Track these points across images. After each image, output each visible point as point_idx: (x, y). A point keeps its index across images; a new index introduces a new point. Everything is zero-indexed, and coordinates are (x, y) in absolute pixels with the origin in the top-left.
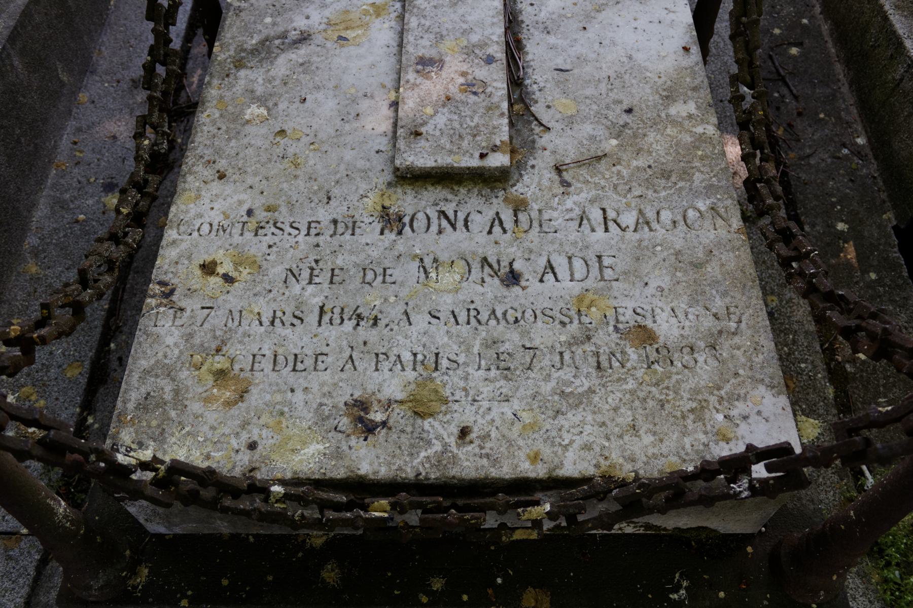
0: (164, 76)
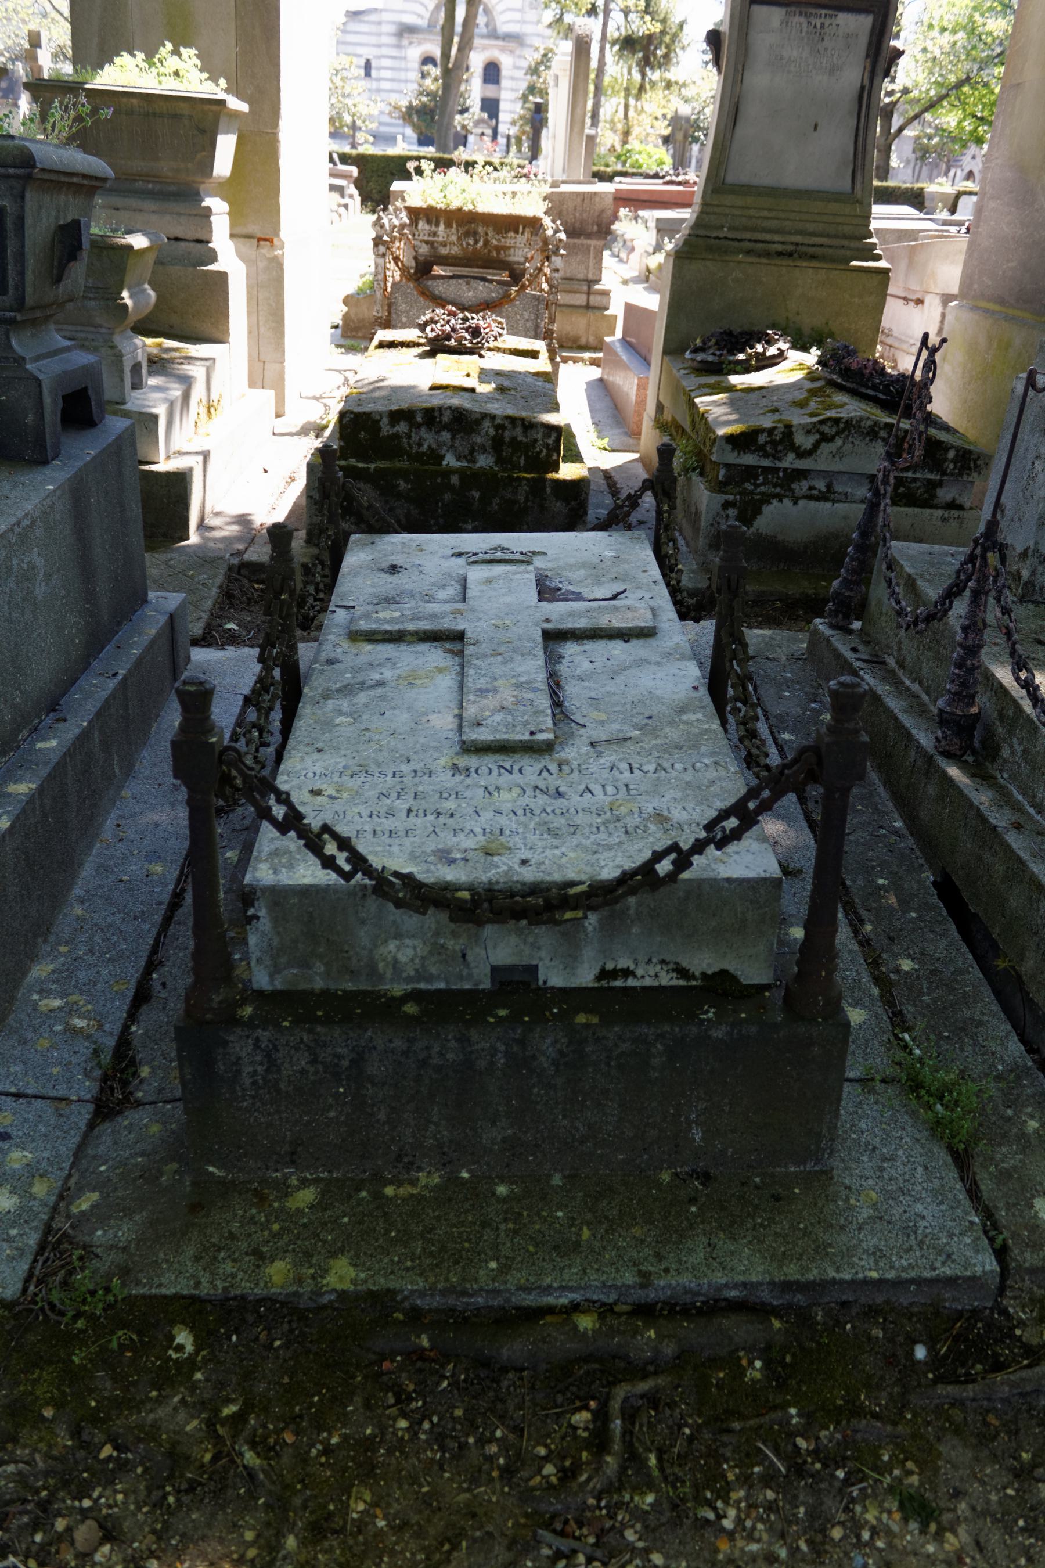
0: (606, 254)
